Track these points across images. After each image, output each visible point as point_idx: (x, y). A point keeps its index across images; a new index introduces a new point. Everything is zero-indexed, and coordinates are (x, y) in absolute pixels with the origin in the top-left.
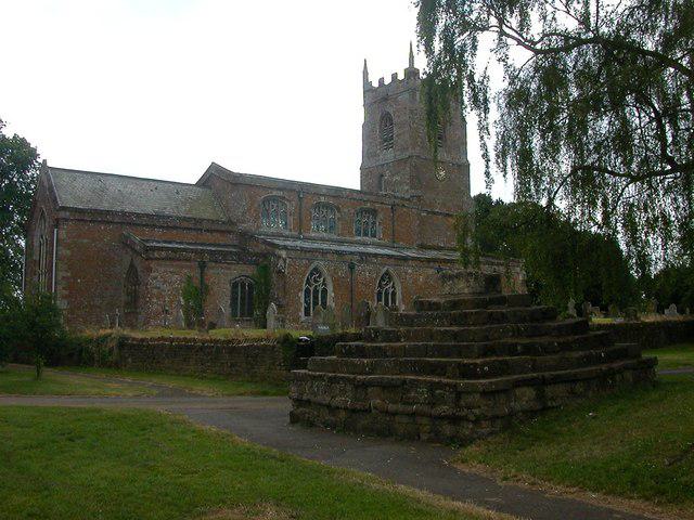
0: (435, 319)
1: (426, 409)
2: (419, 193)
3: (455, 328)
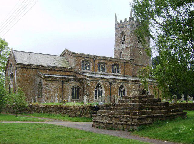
1: (125, 123)
2: (133, 58)
3: (133, 103)
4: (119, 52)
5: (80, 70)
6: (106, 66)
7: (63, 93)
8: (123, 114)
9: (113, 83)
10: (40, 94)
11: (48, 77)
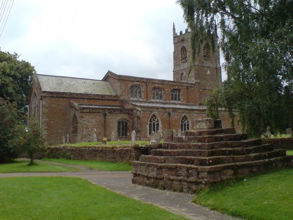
0: (192, 139)
1: (185, 178)
2: (199, 81)
3: (199, 144)
4: (180, 73)
5: (129, 98)
6: (163, 92)
7: (105, 129)
8: (182, 163)
9: (172, 114)
10: (75, 131)
11: (84, 108)
